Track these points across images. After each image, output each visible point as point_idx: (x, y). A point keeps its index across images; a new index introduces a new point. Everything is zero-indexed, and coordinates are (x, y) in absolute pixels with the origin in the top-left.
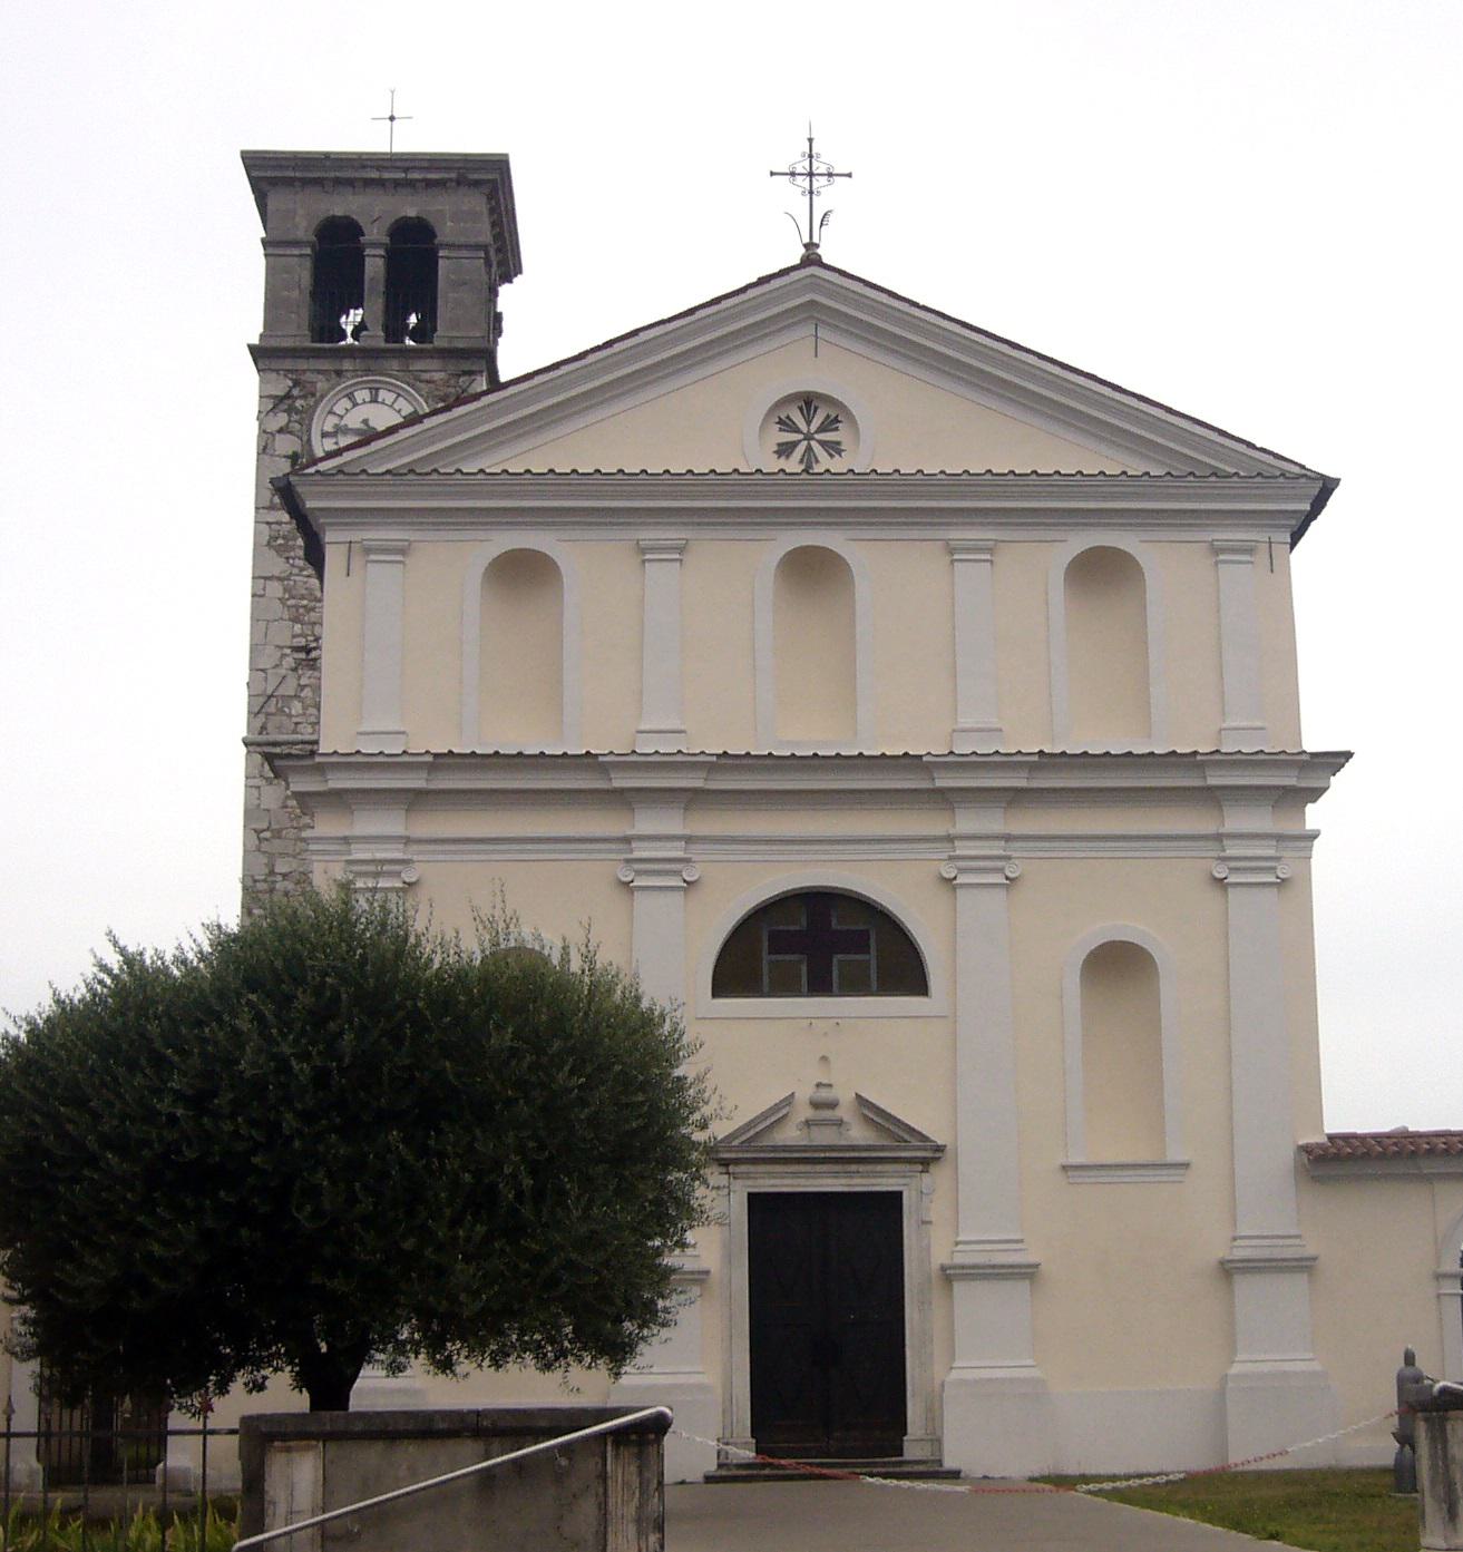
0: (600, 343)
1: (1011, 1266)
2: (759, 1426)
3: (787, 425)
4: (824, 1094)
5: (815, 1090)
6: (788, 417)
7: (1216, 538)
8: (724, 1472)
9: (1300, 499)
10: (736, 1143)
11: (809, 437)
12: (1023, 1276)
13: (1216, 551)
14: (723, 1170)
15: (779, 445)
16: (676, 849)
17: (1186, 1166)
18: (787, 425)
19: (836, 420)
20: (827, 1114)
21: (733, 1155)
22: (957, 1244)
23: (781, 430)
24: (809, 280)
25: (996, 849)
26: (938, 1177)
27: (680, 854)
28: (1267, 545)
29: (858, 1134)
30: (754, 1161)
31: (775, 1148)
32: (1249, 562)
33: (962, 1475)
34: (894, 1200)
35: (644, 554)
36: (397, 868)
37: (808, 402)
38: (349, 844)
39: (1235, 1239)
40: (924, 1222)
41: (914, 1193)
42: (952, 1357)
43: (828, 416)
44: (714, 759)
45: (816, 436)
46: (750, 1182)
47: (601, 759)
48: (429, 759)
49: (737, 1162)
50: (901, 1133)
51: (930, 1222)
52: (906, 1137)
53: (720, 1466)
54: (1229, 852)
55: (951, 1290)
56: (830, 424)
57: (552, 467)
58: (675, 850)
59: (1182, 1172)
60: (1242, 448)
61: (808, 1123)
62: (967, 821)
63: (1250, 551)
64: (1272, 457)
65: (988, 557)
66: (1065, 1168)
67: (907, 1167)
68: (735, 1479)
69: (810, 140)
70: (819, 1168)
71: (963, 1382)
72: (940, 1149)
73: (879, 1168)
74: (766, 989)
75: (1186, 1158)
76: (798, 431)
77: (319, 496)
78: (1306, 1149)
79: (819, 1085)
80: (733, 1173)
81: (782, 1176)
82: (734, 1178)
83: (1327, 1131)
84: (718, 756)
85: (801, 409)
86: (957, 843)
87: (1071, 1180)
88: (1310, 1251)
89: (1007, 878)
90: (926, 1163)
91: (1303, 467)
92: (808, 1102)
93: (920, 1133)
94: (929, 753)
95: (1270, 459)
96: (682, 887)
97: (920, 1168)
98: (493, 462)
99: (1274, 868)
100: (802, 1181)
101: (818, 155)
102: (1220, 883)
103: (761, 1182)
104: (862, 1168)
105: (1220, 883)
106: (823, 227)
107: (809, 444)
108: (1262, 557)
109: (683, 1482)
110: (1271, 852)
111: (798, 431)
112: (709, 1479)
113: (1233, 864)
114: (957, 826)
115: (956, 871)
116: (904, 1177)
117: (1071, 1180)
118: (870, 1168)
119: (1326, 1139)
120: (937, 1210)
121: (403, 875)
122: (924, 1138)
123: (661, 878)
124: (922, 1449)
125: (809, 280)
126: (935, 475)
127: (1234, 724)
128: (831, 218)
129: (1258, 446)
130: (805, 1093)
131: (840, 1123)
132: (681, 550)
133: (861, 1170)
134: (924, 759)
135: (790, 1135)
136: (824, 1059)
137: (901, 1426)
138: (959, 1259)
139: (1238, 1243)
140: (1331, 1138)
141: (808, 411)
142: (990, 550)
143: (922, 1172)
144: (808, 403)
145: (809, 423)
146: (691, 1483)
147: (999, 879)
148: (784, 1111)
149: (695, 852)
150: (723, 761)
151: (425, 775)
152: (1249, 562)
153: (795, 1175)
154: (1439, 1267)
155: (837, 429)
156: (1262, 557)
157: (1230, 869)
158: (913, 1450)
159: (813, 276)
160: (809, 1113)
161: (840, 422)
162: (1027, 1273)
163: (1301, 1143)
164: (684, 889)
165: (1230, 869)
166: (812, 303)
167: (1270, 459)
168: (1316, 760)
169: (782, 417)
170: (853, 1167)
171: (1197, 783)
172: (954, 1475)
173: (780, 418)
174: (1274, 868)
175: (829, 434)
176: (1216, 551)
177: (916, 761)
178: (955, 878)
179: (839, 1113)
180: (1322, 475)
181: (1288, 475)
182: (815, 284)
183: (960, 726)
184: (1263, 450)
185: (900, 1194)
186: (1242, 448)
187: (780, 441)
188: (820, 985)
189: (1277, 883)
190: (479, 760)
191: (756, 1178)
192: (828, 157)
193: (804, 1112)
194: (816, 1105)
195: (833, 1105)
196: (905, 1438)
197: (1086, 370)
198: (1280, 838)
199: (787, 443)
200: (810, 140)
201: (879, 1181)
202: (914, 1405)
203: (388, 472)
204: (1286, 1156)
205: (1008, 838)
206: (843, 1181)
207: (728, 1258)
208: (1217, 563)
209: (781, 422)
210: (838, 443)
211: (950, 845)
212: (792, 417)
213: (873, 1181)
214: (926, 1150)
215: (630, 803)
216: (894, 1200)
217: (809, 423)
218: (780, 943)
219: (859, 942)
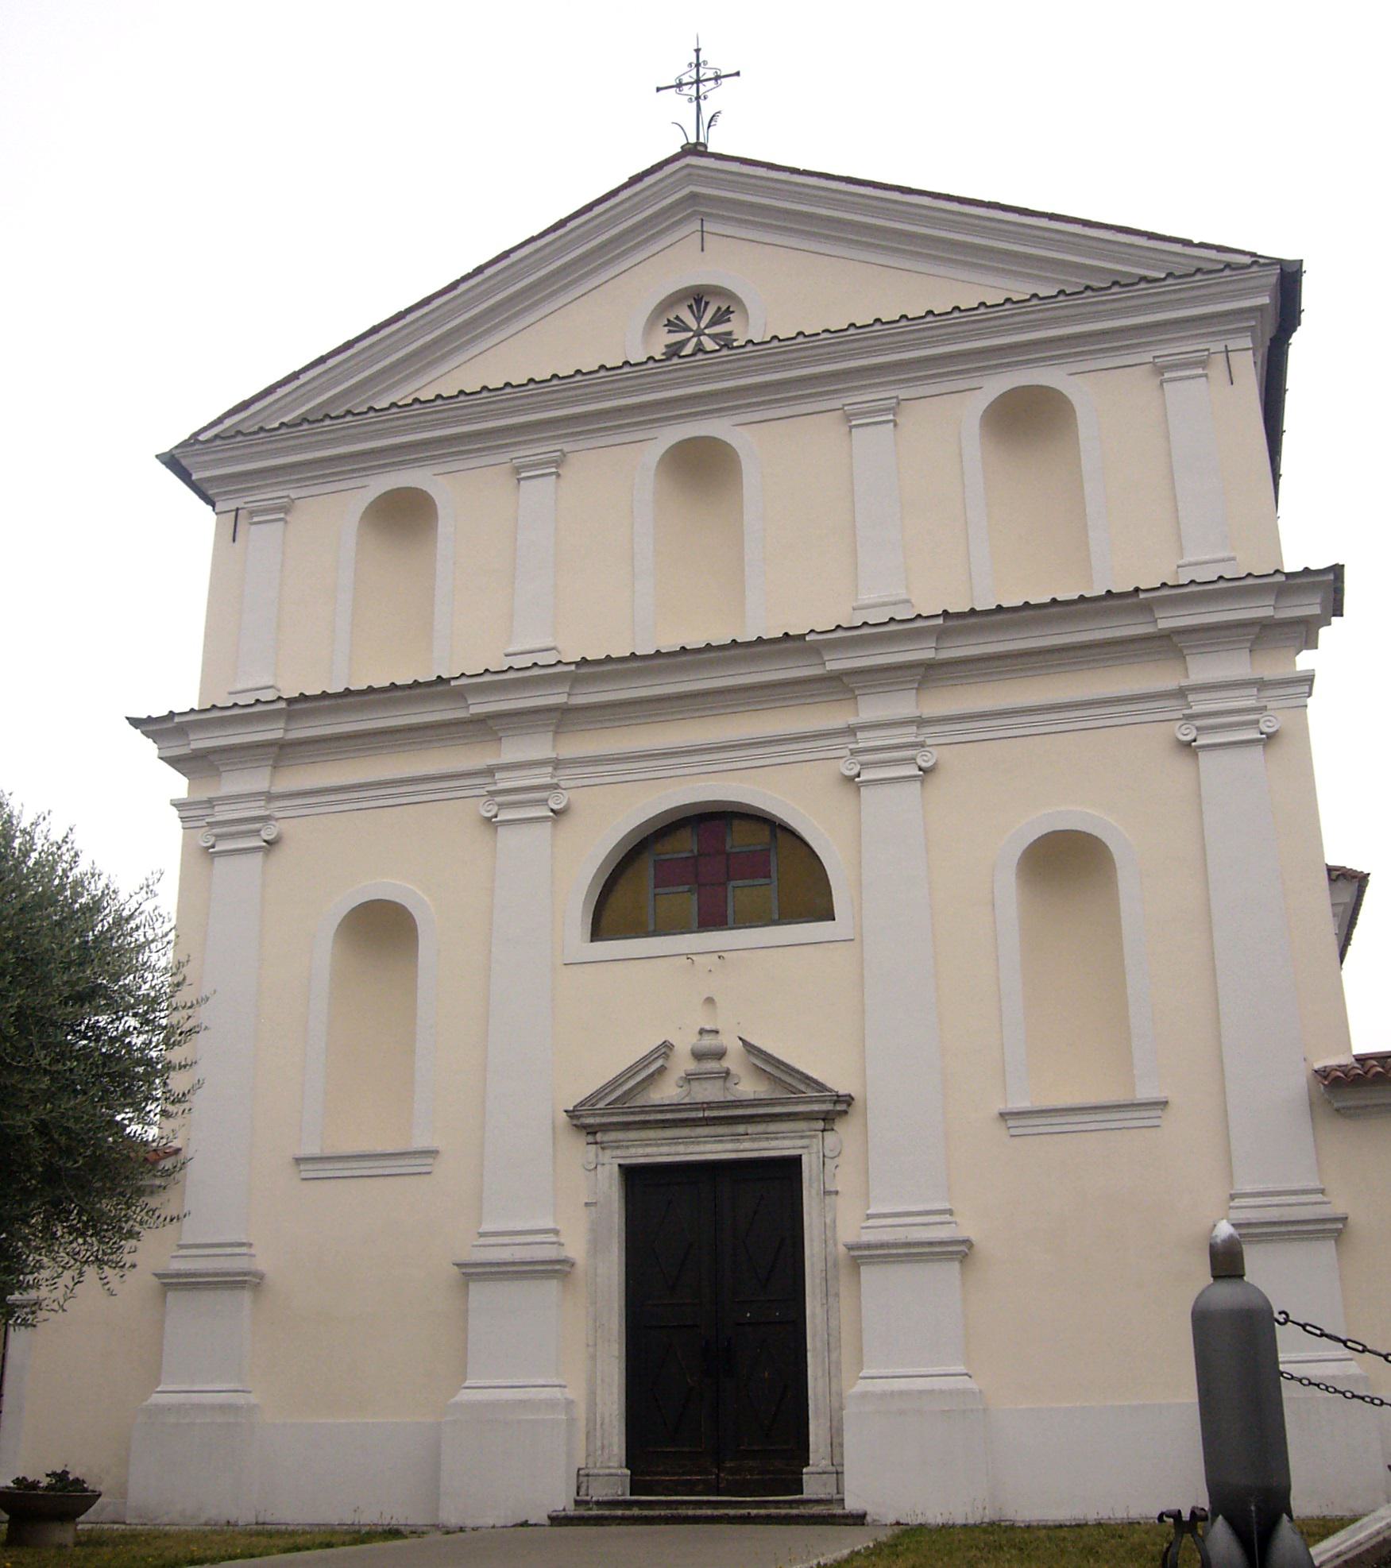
0: (470, 271)
1: (931, 1244)
2: (633, 1457)
3: (676, 325)
4: (708, 1042)
5: (698, 1037)
6: (677, 318)
7: (1158, 353)
8: (582, 1512)
9: (1255, 291)
10: (601, 1105)
11: (699, 333)
12: (949, 1256)
13: (1160, 370)
14: (590, 1139)
15: (667, 346)
16: (544, 775)
17: (1164, 1104)
18: (676, 325)
19: (728, 311)
20: (711, 1065)
21: (598, 1120)
22: (869, 1217)
23: (670, 331)
24: (685, 172)
25: (908, 735)
26: (845, 1132)
27: (548, 780)
28: (1224, 355)
29: (748, 1087)
30: (626, 1126)
31: (644, 1109)
32: (1201, 376)
33: (869, 1519)
34: (791, 1167)
35: (519, 473)
36: (257, 826)
37: (697, 298)
38: (213, 807)
39: (1232, 1197)
40: (826, 1193)
41: (814, 1156)
42: (860, 1365)
43: (719, 308)
44: (573, 667)
45: (707, 331)
46: (618, 1152)
47: (453, 683)
48: (282, 705)
49: (606, 1128)
50: (794, 1083)
51: (837, 1193)
52: (802, 1087)
53: (577, 1503)
54: (1197, 709)
55: (859, 1274)
56: (722, 316)
57: (892, 616)
58: (542, 776)
59: (1159, 1113)
60: (1177, 248)
61: (690, 1078)
62: (872, 708)
63: (1203, 363)
64: (1214, 252)
65: (891, 417)
66: (1003, 1116)
67: (801, 1125)
68: (599, 1521)
69: (698, 51)
70: (700, 1131)
71: (864, 1395)
72: (849, 1100)
73: (773, 1127)
74: (651, 928)
75: (1163, 1095)
76: (687, 329)
77: (205, 466)
78: (1323, 1074)
79: (702, 1032)
80: (602, 1143)
81: (657, 1142)
82: (603, 1148)
83: (1354, 1053)
84: (577, 663)
85: (690, 307)
86: (860, 735)
87: (1013, 1131)
88: (1338, 1208)
89: (920, 769)
90: (828, 1119)
91: (1253, 255)
92: (690, 1052)
93: (816, 1082)
94: (812, 631)
95: (1212, 254)
96: (549, 817)
97: (821, 1125)
98: (402, 394)
99: (1257, 722)
100: (681, 1149)
101: (705, 62)
102: (1188, 747)
103: (633, 1151)
104: (751, 1129)
105: (1188, 747)
106: (711, 128)
107: (699, 340)
108: (1218, 370)
109: (525, 1524)
110: (1251, 703)
111: (687, 329)
112: (556, 1520)
113: (1199, 723)
114: (860, 715)
115: (859, 767)
116: (802, 1137)
117: (1013, 1131)
118: (761, 1128)
119: (1353, 1060)
120: (844, 1179)
121: (262, 833)
122: (821, 1087)
123: (533, 809)
124: (825, 1485)
125: (685, 172)
126: (818, 334)
127: (1192, 559)
128: (720, 119)
129: (1196, 241)
130: (685, 1042)
131: (727, 1074)
132: (558, 463)
133: (749, 1132)
134: (807, 638)
135: (668, 1092)
136: (710, 1000)
137: (800, 1452)
138: (868, 1237)
139: (1237, 1202)
140: (1361, 1059)
141: (699, 311)
142: (892, 410)
143: (823, 1131)
144: (698, 301)
145: (699, 319)
146: (535, 1525)
147: (257, 843)
148: (659, 1063)
149: (564, 777)
150: (584, 670)
151: (282, 725)
152: (1201, 376)
153: (675, 1140)
154: (1232, 1189)
155: (729, 320)
156: (1218, 370)
157: (1198, 729)
158: (813, 1486)
159: (688, 166)
160: (691, 1066)
161: (733, 312)
162: (961, 1252)
163: (1317, 1066)
164: (555, 822)
165: (1198, 729)
166: (693, 196)
167: (1212, 254)
168: (1292, 582)
169: (672, 319)
170: (741, 1129)
171: (1148, 629)
172: (859, 1519)
173: (669, 320)
174: (1257, 722)
175: (724, 325)
176: (1160, 370)
177: (798, 644)
178: (858, 775)
179: (726, 1063)
180: (1278, 259)
181: (1233, 266)
182: (691, 176)
183: (860, 603)
184: (1202, 245)
185: (796, 1161)
186: (1177, 248)
187: (668, 343)
188: (713, 919)
189: (1262, 739)
190: (332, 702)
191: (627, 1147)
192: (715, 60)
193: (682, 1064)
194: (699, 1056)
195: (720, 1055)
196: (805, 1470)
197: (986, 199)
198: (1262, 684)
199: (675, 344)
200: (698, 51)
201: (774, 1144)
202: (816, 1435)
203: (304, 420)
204: (1296, 1084)
205: (921, 722)
206: (730, 1146)
207: (595, 1247)
208: (1161, 383)
209: (670, 323)
210: (730, 333)
211: (852, 739)
212: (682, 318)
213: (764, 1144)
214: (824, 1102)
215: (852, 690)
216: (791, 1167)
217: (699, 319)
218: (666, 876)
219: (755, 866)
